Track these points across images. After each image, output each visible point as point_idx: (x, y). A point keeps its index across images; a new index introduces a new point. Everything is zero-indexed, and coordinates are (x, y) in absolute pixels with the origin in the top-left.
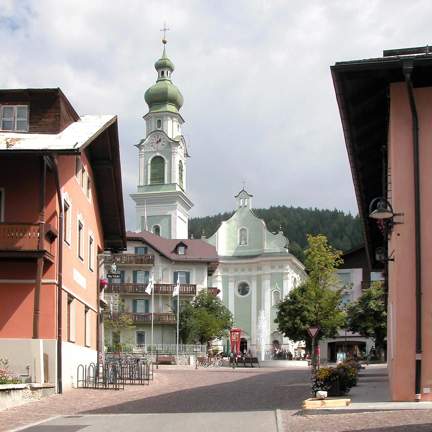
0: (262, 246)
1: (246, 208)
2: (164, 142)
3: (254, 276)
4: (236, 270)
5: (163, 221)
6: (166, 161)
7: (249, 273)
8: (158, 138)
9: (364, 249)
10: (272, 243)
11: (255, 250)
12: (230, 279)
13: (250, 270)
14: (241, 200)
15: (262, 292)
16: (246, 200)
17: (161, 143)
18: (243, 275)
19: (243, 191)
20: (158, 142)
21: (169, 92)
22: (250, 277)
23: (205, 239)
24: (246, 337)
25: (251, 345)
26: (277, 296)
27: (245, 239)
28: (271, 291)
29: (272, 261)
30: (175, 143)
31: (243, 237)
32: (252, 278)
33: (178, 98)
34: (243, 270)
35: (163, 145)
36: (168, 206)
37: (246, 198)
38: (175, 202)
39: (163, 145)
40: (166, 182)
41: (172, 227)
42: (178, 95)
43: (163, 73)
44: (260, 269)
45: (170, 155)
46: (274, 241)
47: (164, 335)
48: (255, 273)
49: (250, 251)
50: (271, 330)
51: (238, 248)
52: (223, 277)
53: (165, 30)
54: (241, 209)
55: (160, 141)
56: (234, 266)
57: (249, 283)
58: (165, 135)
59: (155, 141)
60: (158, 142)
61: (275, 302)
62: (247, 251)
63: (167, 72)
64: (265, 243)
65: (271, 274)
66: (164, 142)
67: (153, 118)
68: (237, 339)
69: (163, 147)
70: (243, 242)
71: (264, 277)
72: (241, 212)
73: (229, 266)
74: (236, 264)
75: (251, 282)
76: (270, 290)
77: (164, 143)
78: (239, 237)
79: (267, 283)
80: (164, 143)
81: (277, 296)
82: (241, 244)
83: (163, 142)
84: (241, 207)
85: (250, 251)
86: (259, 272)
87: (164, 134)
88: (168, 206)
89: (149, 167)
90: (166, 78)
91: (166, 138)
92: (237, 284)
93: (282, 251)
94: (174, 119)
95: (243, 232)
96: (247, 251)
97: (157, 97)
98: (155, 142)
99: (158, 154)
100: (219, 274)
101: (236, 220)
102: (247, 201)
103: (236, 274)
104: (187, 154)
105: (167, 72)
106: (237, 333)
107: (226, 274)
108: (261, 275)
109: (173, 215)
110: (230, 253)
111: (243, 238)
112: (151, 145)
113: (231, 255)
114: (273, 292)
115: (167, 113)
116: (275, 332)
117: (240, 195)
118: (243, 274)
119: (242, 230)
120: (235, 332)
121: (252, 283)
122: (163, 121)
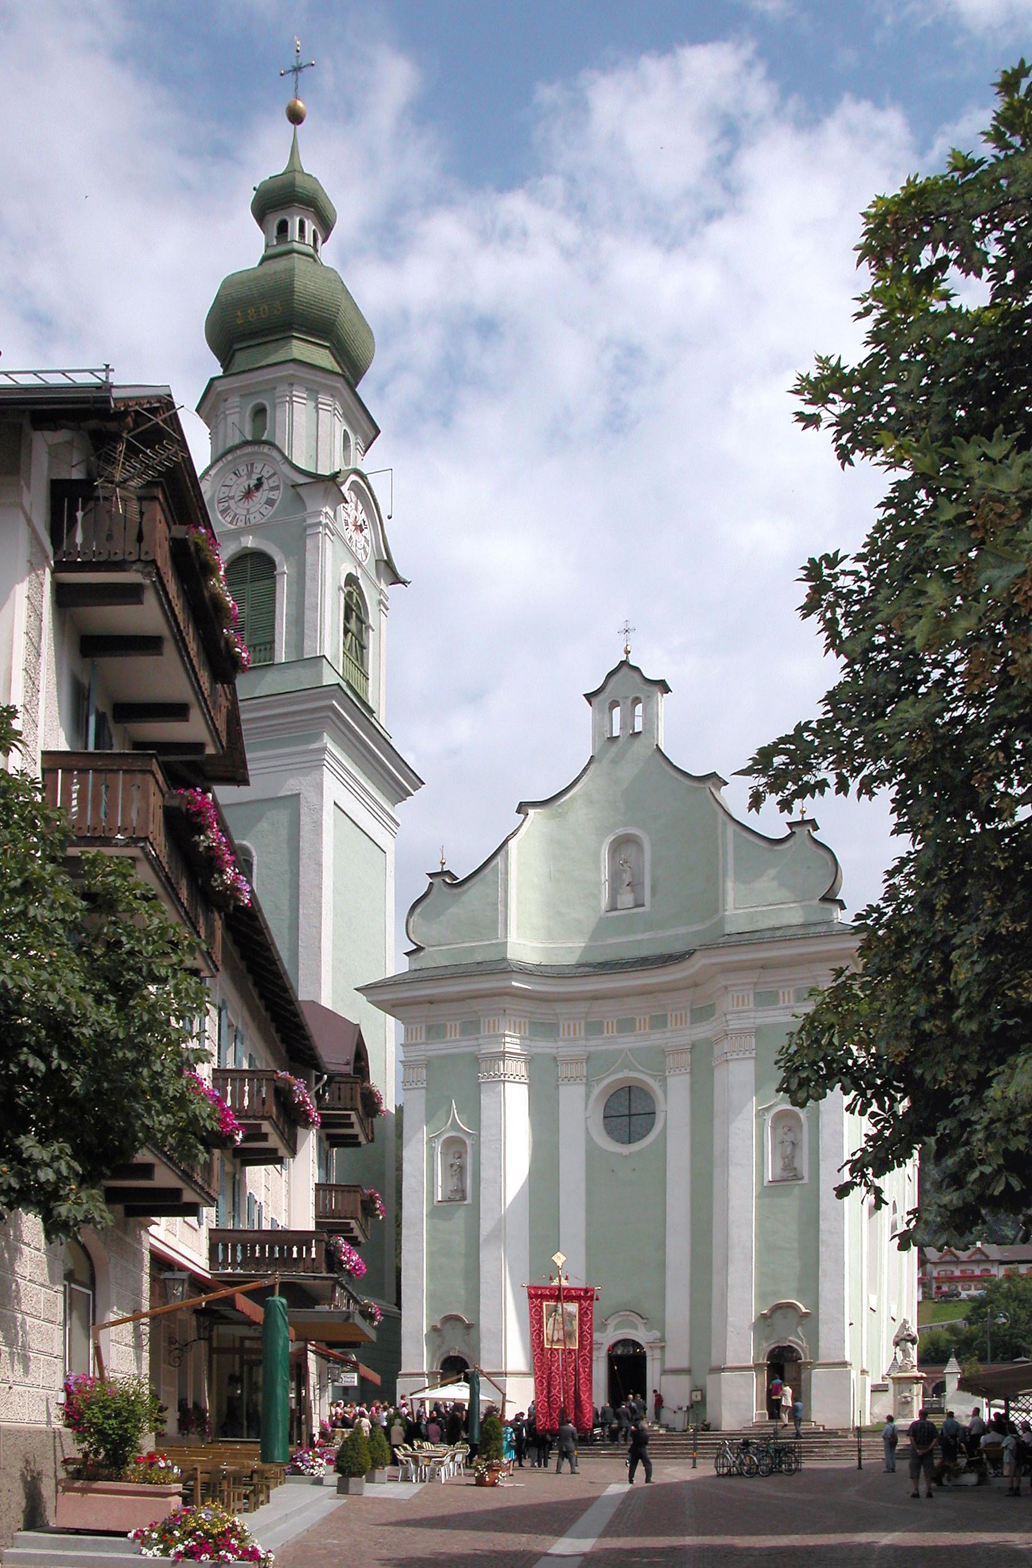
0: (714, 905)
1: (638, 745)
3: (678, 1051)
4: (594, 1028)
5: (264, 825)
6: (284, 568)
7: (657, 1038)
8: (249, 475)
10: (760, 885)
11: (682, 930)
12: (564, 1070)
13: (659, 1022)
14: (617, 711)
15: (717, 1122)
16: (639, 708)
17: (261, 496)
19: (625, 669)
20: (248, 494)
21: (298, 285)
22: (658, 1060)
23: (446, 890)
24: (641, 1335)
26: (790, 1137)
27: (634, 886)
28: (761, 1114)
29: (764, 966)
30: (321, 487)
31: (625, 877)
32: (670, 1060)
33: (341, 318)
34: (626, 1026)
35: (270, 502)
37: (636, 701)
38: (318, 737)
39: (270, 502)
40: (281, 655)
41: (304, 845)
42: (344, 303)
43: (283, 228)
44: (702, 1013)
45: (300, 539)
46: (772, 872)
48: (681, 1034)
49: (660, 934)
50: (761, 1297)
51: (602, 929)
52: (531, 1061)
54: (614, 749)
55: (259, 485)
56: (583, 1007)
57: (654, 1084)
58: (279, 457)
59: (238, 491)
60: (248, 494)
61: (780, 1164)
62: (646, 936)
63: (302, 224)
64: (730, 884)
66: (276, 488)
67: (235, 400)
68: (568, 1335)
69: (269, 511)
70: (626, 899)
71: (726, 1046)
72: (615, 762)
73: (561, 1008)
74: (595, 997)
75: (663, 1081)
76: (753, 1106)
77: (274, 495)
78: (605, 875)
80: (274, 495)
81: (790, 1137)
82: (615, 909)
83: (272, 489)
84: (613, 739)
85: (660, 934)
86: (703, 1031)
87: (275, 454)
90: (296, 246)
91: (286, 469)
92: (597, 1090)
93: (813, 919)
94: (323, 398)
95: (630, 851)
96: (646, 936)
97: (251, 311)
98: (239, 495)
99: (249, 542)
100: (512, 1044)
101: (590, 802)
102: (644, 709)
103: (596, 1044)
104: (389, 564)
105: (302, 224)
106: (573, 1308)
107: (544, 1046)
108: (709, 1044)
109: (308, 796)
110: (570, 950)
111: (627, 878)
112: (222, 507)
113: (571, 959)
114: (769, 1118)
115: (290, 370)
116: (779, 1307)
117: (608, 688)
118: (627, 1042)
119: (622, 844)
120: (558, 1299)
121: (672, 1081)
122: (274, 406)
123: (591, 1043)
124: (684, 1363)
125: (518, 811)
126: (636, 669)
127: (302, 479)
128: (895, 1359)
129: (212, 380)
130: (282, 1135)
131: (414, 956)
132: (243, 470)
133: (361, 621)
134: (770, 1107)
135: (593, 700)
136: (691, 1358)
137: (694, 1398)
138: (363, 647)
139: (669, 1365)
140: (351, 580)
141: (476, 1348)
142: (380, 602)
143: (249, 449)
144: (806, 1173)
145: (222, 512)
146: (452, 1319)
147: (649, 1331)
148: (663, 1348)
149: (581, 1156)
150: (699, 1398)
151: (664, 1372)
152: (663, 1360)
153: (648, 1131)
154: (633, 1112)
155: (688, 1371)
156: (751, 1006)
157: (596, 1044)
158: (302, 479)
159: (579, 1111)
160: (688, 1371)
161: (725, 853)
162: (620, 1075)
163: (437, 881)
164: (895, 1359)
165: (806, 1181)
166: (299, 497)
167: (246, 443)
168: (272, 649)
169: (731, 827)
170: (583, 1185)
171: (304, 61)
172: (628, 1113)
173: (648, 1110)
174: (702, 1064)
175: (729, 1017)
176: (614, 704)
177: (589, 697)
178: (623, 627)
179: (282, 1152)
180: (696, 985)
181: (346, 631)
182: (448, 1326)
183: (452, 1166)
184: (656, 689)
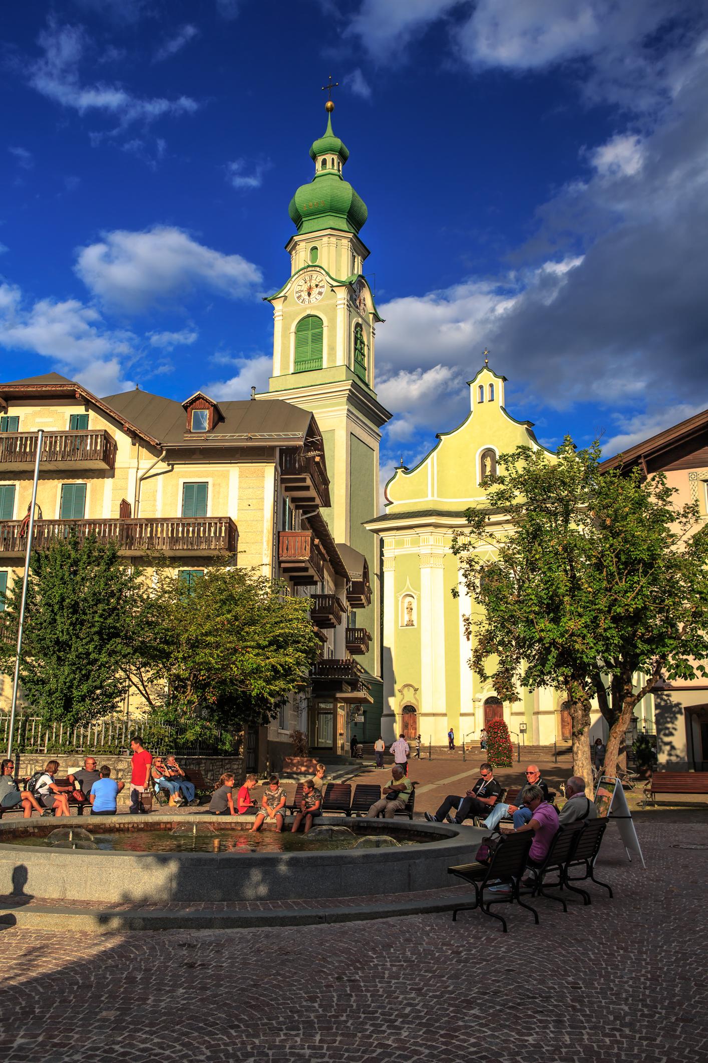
25: (473, 715)
89: (292, 337)
127: (335, 284)
151: (512, 714)
158: (335, 284)
163: (399, 471)
168: (321, 361)
182: (406, 689)
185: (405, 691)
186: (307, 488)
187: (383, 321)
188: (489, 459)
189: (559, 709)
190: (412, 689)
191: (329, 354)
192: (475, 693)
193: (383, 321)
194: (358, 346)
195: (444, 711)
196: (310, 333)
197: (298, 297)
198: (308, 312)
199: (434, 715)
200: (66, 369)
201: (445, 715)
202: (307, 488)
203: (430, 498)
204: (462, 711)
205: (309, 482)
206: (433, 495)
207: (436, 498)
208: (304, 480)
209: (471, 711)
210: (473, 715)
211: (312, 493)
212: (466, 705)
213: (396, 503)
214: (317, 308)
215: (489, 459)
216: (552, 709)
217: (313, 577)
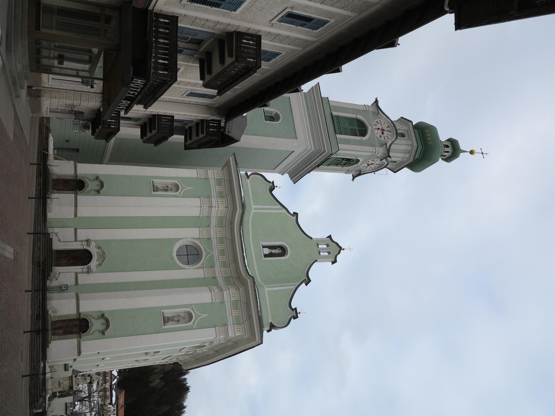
2: (385, 139)
9: (54, 329)
18: (214, 252)
19: (339, 249)
24: (93, 264)
25: (76, 240)
34: (222, 252)
36: (309, 133)
37: (329, 253)
47: (75, 312)
48: (219, 272)
50: (112, 312)
53: (482, 153)
63: (448, 152)
65: (223, 302)
71: (217, 290)
79: (204, 296)
86: (221, 281)
87: (394, 139)
88: (309, 133)
89: (353, 116)
103: (214, 242)
104: (360, 174)
105: (448, 152)
114: (189, 310)
117: (333, 244)
118: (216, 253)
123: (215, 239)
124: (80, 282)
125: (294, 213)
126: (339, 253)
127: (388, 146)
128: (81, 372)
129: (411, 122)
130: (151, 137)
131: (245, 175)
132: (389, 129)
133: (345, 164)
134: (194, 311)
135: (328, 239)
136: (83, 285)
137: (63, 287)
138: (337, 165)
139: (79, 275)
140: (358, 161)
141: (89, 193)
142: (349, 171)
143: (395, 131)
144: (166, 327)
145: (377, 122)
146: (102, 185)
147: (96, 266)
148: (88, 272)
149: (172, 237)
150: (63, 288)
151: (76, 274)
152: (82, 273)
153: (181, 262)
154: (189, 256)
155: (77, 283)
156: (232, 300)
157: (214, 242)
158: (388, 146)
159: (189, 235)
160: (77, 283)
161: (281, 286)
162: (203, 251)
163: (271, 184)
164: (81, 372)
165: (163, 327)
166: (383, 146)
167: (396, 130)
168: (340, 134)
169: (294, 288)
170: (159, 237)
171: (485, 155)
172: (191, 254)
173: (190, 262)
174: (209, 282)
175: (228, 291)
176: (328, 245)
177: (330, 237)
178: (351, 248)
179: (145, 138)
180: (239, 278)
181: (343, 159)
182: (98, 183)
183: (167, 187)
184: (333, 260)
185: (97, 182)
186: (197, 135)
187: (353, 179)
188: (280, 251)
189: (82, 317)
190: (98, 188)
191: (345, 139)
192: (95, 241)
193: (353, 179)
194: (344, 162)
195: (78, 215)
196: (357, 128)
197: (377, 122)
198: (370, 128)
199: (76, 206)
200: (195, 56)
201: (76, 215)
202: (197, 135)
203: (254, 207)
204: (78, 231)
205: (201, 136)
206: (255, 209)
207: (253, 211)
208: (203, 133)
209: (78, 239)
210: (76, 240)
211: (195, 138)
212: (83, 234)
213: (248, 181)
214: (373, 133)
215: (280, 251)
216: (82, 310)
217: (146, 136)
